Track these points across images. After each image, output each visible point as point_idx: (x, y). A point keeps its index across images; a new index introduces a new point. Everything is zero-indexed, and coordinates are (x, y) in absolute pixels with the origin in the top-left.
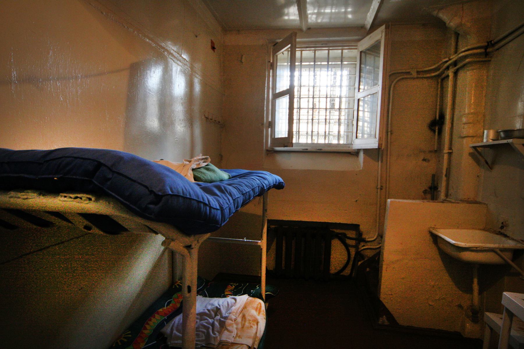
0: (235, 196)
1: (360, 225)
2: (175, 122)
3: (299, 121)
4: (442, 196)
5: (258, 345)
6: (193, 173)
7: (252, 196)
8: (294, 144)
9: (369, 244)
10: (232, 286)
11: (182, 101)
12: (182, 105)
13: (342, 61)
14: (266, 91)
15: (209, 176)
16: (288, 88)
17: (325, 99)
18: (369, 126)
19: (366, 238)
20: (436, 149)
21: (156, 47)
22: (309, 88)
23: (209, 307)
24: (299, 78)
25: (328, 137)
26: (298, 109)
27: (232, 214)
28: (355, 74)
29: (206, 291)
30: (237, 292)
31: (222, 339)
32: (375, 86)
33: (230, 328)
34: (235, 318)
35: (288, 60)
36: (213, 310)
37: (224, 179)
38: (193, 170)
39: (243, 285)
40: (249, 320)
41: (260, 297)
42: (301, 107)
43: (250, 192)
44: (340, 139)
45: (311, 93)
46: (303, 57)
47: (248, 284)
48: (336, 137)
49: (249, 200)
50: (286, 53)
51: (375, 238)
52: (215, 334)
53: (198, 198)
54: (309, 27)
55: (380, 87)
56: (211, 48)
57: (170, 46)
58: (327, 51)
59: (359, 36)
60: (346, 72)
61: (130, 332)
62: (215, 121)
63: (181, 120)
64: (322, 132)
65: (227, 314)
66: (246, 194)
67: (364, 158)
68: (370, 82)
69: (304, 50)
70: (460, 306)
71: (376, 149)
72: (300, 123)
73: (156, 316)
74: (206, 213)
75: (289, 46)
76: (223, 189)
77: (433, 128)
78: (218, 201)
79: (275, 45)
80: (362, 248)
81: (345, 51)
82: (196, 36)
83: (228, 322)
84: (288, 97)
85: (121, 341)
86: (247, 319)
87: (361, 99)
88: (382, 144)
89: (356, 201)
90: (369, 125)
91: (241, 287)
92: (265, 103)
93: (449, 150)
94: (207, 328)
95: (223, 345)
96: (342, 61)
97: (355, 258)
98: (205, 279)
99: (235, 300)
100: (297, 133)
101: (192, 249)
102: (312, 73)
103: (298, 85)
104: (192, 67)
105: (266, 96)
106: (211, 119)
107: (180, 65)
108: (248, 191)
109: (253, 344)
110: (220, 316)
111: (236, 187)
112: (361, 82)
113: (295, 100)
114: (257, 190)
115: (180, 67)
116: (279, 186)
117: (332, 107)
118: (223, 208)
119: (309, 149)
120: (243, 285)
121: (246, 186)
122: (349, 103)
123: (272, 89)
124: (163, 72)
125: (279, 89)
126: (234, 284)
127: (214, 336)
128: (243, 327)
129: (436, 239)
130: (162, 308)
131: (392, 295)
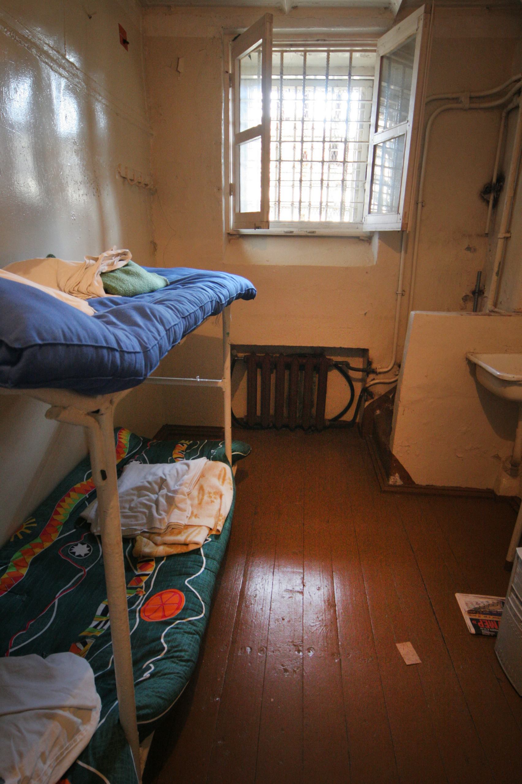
0: (170, 324)
1: (369, 349)
2: (68, 186)
3: (279, 183)
4: (489, 305)
5: (222, 526)
6: (102, 280)
7: (200, 318)
8: (270, 224)
9: (381, 376)
10: (183, 446)
11: (75, 147)
12: (77, 155)
13: (350, 75)
14: (223, 128)
15: (130, 285)
16: (260, 123)
17: (321, 143)
18: (390, 193)
19: (377, 368)
20: (486, 232)
21: (13, 38)
22: (295, 124)
23: (150, 478)
24: (279, 105)
25: (325, 210)
26: (278, 163)
27: (167, 353)
28: (372, 100)
29: (144, 455)
30: (190, 454)
31: (170, 522)
32: (402, 123)
33: (181, 505)
34: (189, 491)
35: (259, 71)
36: (156, 482)
37: (156, 288)
38: (102, 274)
39: (199, 442)
40: (210, 493)
41: (224, 460)
42: (283, 159)
43: (196, 312)
44: (344, 214)
45: (299, 133)
46: (284, 65)
47: (206, 441)
48: (337, 211)
49: (195, 326)
50: (255, 55)
51: (390, 368)
52: (160, 515)
53: (96, 341)
54: (294, 5)
55: (409, 126)
56: (121, 41)
57: (40, 36)
58: (325, 54)
59: (379, 26)
60: (356, 94)
61: (34, 520)
62: (140, 183)
63: (78, 182)
64: (316, 203)
65: (177, 486)
66: (189, 317)
67: (380, 247)
68: (395, 113)
69: (286, 51)
70: (497, 457)
71: (399, 231)
72: (281, 187)
73: (72, 494)
74: (114, 362)
75: (261, 41)
76: (149, 312)
77: (486, 196)
78: (138, 337)
79: (236, 38)
80: (372, 383)
81: (356, 55)
82: (90, 18)
83: (179, 497)
84: (260, 140)
85: (22, 533)
86: (206, 492)
87: (379, 145)
88: (407, 224)
89: (365, 314)
90: (389, 191)
91: (196, 447)
92: (223, 151)
93: (506, 233)
94: (149, 508)
95: (173, 528)
96: (350, 75)
97: (361, 397)
98: (142, 437)
99: (188, 465)
100: (275, 203)
101: (102, 414)
102: (300, 95)
103: (277, 118)
104: (88, 80)
105: (223, 137)
106: (131, 180)
107: (64, 77)
108: (193, 311)
109: (216, 524)
110: (167, 489)
111: (172, 305)
112: (380, 114)
113: (273, 146)
114: (209, 308)
115: (65, 80)
116: (248, 295)
117: (333, 161)
118: (147, 348)
119: (296, 231)
120: (199, 442)
121: (190, 301)
122: (360, 152)
123: (232, 124)
124: (32, 90)
125: (246, 126)
126: (187, 442)
127: (160, 517)
128: (200, 504)
129: (474, 367)
130: (80, 482)
131: (409, 446)
